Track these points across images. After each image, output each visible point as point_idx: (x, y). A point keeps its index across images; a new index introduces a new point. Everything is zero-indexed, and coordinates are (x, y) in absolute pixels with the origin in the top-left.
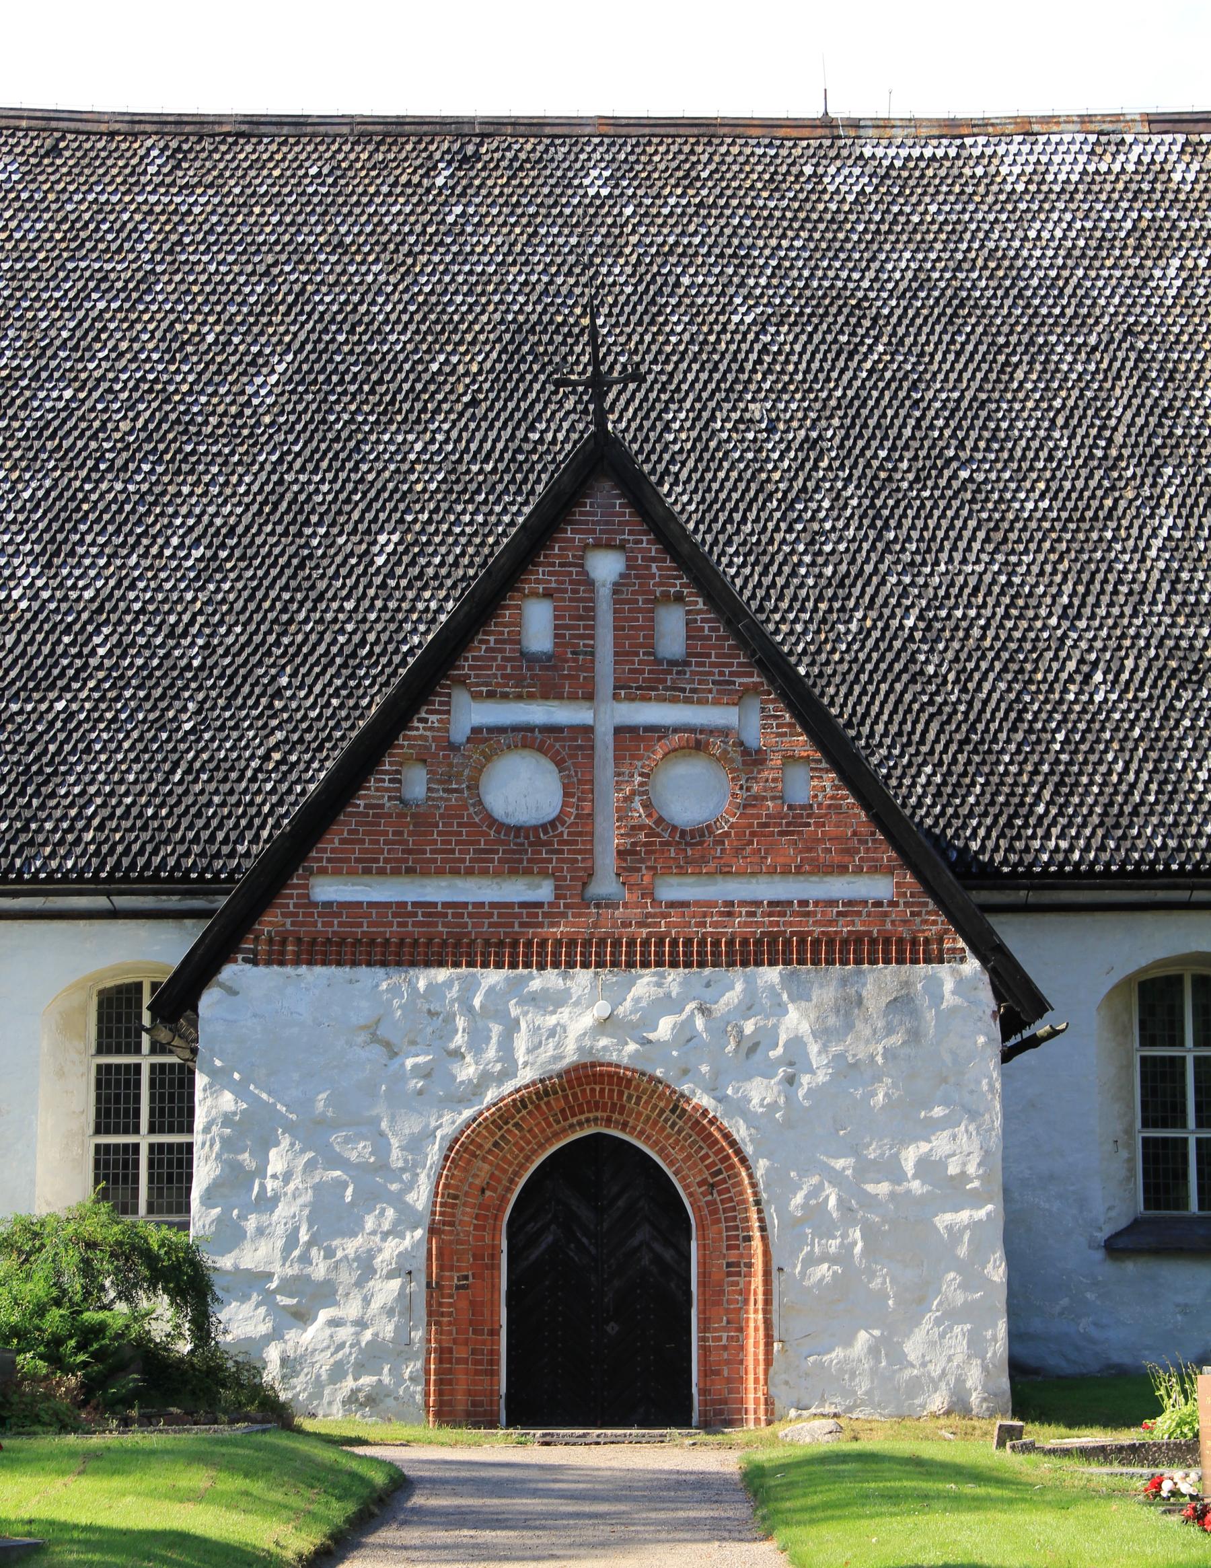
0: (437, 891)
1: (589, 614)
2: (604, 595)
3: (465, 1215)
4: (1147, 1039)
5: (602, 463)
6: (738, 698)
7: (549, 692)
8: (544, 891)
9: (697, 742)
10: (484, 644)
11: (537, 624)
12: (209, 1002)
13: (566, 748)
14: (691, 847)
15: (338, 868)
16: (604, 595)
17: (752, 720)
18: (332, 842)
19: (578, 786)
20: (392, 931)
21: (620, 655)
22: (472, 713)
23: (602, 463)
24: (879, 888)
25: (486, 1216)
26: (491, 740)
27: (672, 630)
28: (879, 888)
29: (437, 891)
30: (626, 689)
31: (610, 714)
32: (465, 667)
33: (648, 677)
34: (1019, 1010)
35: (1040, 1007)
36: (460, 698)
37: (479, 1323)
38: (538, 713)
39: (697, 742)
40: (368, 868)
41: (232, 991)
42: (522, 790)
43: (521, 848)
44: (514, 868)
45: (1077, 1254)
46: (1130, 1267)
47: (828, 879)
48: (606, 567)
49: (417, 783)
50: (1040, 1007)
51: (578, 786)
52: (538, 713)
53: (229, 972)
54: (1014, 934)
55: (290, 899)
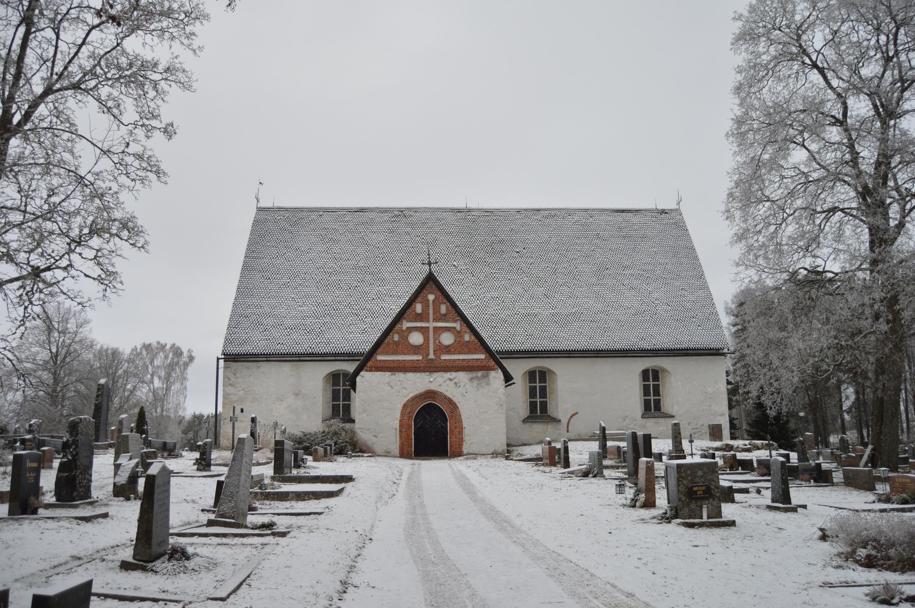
0: (400, 358)
1: (428, 306)
2: (431, 302)
3: (406, 418)
4: (644, 381)
5: (430, 281)
6: (455, 321)
7: (421, 321)
8: (420, 358)
9: (447, 329)
10: (409, 311)
11: (419, 308)
12: (358, 379)
13: (424, 331)
14: (448, 349)
15: (382, 353)
16: (431, 302)
17: (457, 325)
18: (380, 349)
19: (426, 339)
20: (392, 365)
21: (434, 314)
22: (406, 325)
23: (430, 281)
24: (482, 356)
25: (410, 418)
26: (410, 330)
27: (443, 309)
28: (482, 356)
29: (400, 358)
30: (435, 320)
31: (432, 325)
32: (405, 315)
33: (440, 318)
34: (508, 378)
35: (512, 378)
36: (404, 322)
37: (409, 438)
38: (419, 324)
39: (447, 329)
40: (387, 354)
41: (739, 17)
42: (416, 339)
43: (416, 349)
44: (415, 353)
45: (518, 422)
46: (527, 425)
47: (397, 374)
48: (431, 297)
49: (396, 338)
50: (512, 378)
51: (426, 339)
52: (419, 324)
53: (362, 373)
54: (505, 363)
55: (373, 359)
